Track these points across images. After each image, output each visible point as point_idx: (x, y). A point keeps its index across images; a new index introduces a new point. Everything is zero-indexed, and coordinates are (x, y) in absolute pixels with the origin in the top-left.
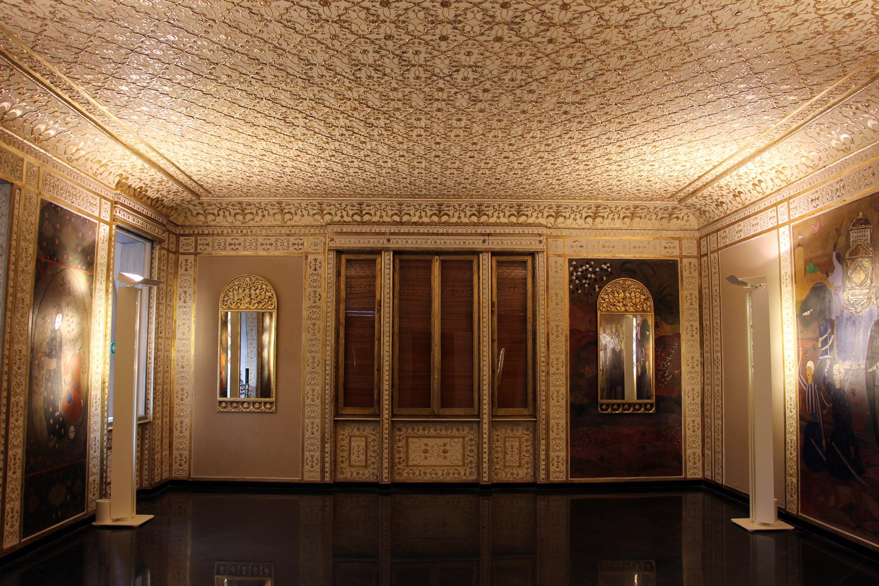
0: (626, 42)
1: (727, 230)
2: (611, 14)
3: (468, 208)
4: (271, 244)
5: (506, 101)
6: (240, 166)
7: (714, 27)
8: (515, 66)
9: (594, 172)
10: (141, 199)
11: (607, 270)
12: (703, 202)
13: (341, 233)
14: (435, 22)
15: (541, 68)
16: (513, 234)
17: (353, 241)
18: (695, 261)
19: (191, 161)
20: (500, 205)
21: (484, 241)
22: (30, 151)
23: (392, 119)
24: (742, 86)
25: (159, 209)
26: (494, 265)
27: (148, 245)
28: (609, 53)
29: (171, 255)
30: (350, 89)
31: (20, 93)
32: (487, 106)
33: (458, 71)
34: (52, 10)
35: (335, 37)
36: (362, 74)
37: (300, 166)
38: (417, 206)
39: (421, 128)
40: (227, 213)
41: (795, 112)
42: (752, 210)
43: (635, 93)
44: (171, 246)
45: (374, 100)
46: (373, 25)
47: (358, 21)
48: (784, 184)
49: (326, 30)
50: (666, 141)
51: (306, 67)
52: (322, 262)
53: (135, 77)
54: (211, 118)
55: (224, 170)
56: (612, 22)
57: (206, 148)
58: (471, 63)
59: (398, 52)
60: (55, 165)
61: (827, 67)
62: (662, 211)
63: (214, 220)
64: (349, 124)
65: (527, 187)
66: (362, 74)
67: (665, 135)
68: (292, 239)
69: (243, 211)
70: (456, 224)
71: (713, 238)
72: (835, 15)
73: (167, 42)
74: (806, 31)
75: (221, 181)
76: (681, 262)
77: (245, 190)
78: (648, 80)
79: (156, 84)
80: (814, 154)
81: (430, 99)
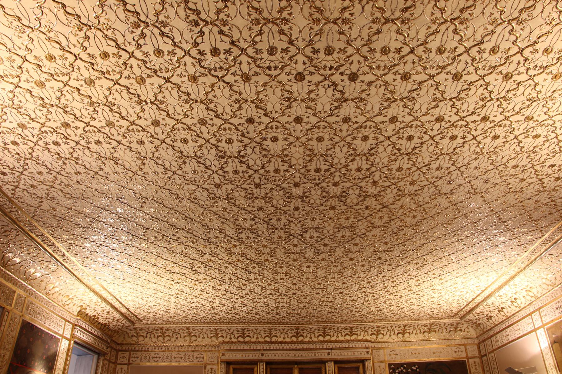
0: (417, 206)
1: (498, 336)
2: (405, 187)
3: (317, 331)
4: (181, 358)
5: (339, 252)
6: (162, 302)
7: (473, 191)
8: (344, 227)
9: (401, 300)
10: (94, 323)
11: (416, 370)
12: (477, 317)
13: (230, 350)
14: (290, 197)
15: (362, 227)
16: (349, 348)
17: (238, 355)
18: (478, 360)
19: (129, 298)
20: (338, 328)
21: (329, 354)
22: (21, 286)
23: (263, 267)
24: (495, 231)
25: (106, 331)
26: (336, 371)
27: (96, 357)
28: (405, 214)
29: (111, 365)
30: (235, 246)
31: (21, 248)
32: (327, 256)
33: (306, 232)
34: (47, 192)
35: (225, 209)
36: (243, 236)
37: (203, 302)
38: (282, 331)
39: (283, 273)
40: (152, 336)
41: (532, 248)
42: (513, 320)
43: (425, 241)
44: (112, 358)
45: (251, 254)
46: (250, 201)
47: (240, 198)
48: (533, 299)
49: (219, 204)
50: (448, 274)
51: (206, 231)
52: (217, 371)
53: (95, 237)
54: (143, 267)
55: (151, 304)
56: (406, 192)
57: (139, 288)
58: (315, 226)
59: (266, 220)
60: (37, 297)
61: (549, 214)
62: (450, 326)
63: (143, 341)
64: (235, 271)
65: (356, 314)
66: (243, 236)
67: (447, 270)
68: (196, 354)
69: (163, 334)
70: (309, 342)
71: (488, 342)
72: (549, 179)
73: (116, 213)
74: (532, 191)
75: (149, 313)
76: (468, 362)
77: (165, 319)
78: (433, 232)
79: (108, 242)
80: (550, 276)
81: (289, 253)
